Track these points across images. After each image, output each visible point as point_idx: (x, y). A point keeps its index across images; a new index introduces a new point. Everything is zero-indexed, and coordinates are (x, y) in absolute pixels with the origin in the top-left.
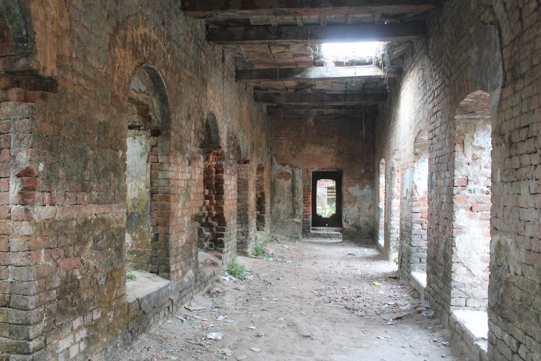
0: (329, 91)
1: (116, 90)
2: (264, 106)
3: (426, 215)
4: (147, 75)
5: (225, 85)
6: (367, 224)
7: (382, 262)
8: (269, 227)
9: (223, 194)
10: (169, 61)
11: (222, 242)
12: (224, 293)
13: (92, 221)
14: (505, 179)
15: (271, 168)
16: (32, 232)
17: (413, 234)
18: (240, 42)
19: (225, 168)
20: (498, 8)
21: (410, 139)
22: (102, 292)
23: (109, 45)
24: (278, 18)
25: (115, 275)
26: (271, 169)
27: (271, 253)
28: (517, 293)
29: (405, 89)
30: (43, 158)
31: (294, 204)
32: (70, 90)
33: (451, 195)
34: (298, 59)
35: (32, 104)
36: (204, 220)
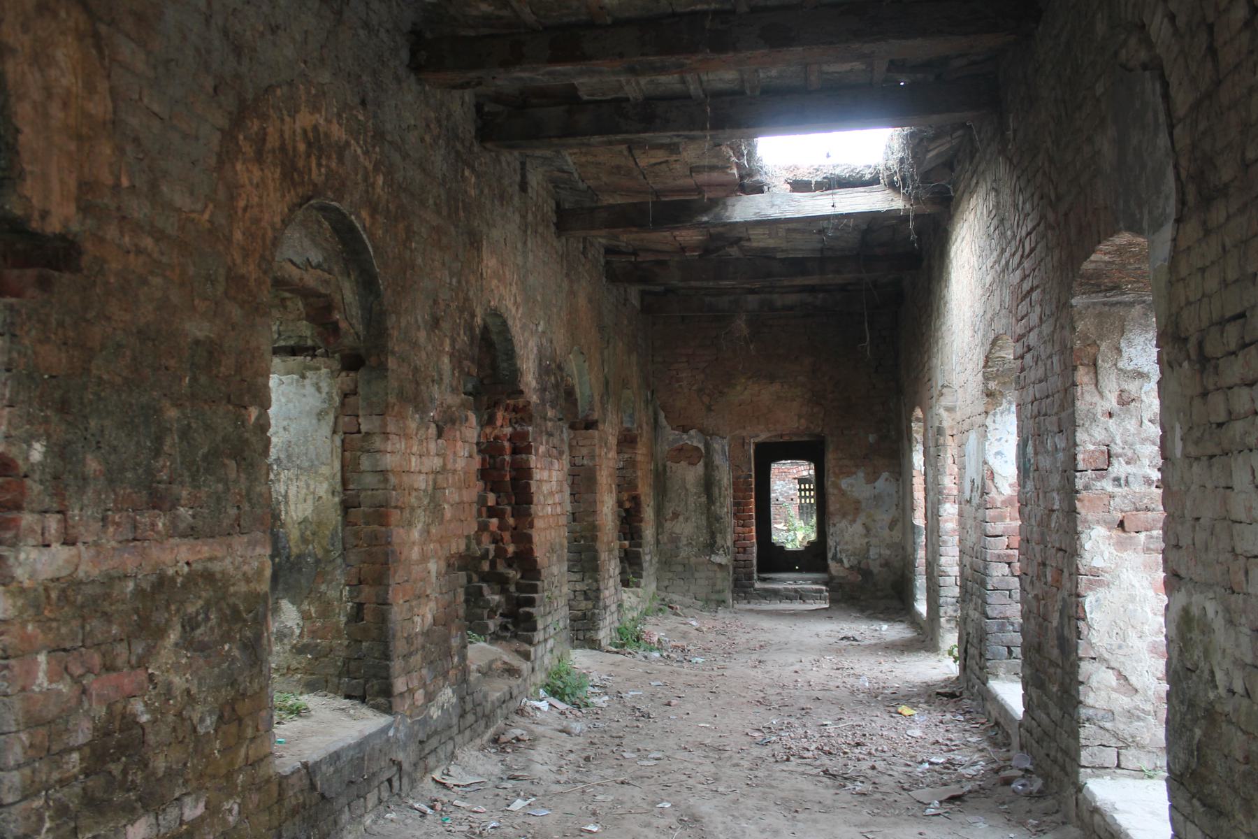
0: (783, 251)
1: (239, 261)
2: (634, 293)
3: (1015, 542)
4: (326, 224)
5: (529, 244)
6: (886, 564)
7: (923, 655)
8: (653, 578)
9: (531, 502)
10: (378, 190)
11: (530, 616)
12: (533, 741)
13: (179, 580)
14: (1192, 450)
15: (656, 439)
16: (11, 613)
17: (990, 587)
18: (556, 141)
19: (535, 440)
20: (1159, 27)
21: (975, 358)
22: (207, 751)
23: (219, 155)
24: (643, 81)
25: (243, 707)
26: (655, 439)
27: (656, 639)
28: (1238, 743)
29: (959, 240)
30: (41, 431)
31: (713, 521)
32: (114, 265)
33: (1070, 493)
34: (703, 177)
35: (13, 300)
36: (486, 566)
